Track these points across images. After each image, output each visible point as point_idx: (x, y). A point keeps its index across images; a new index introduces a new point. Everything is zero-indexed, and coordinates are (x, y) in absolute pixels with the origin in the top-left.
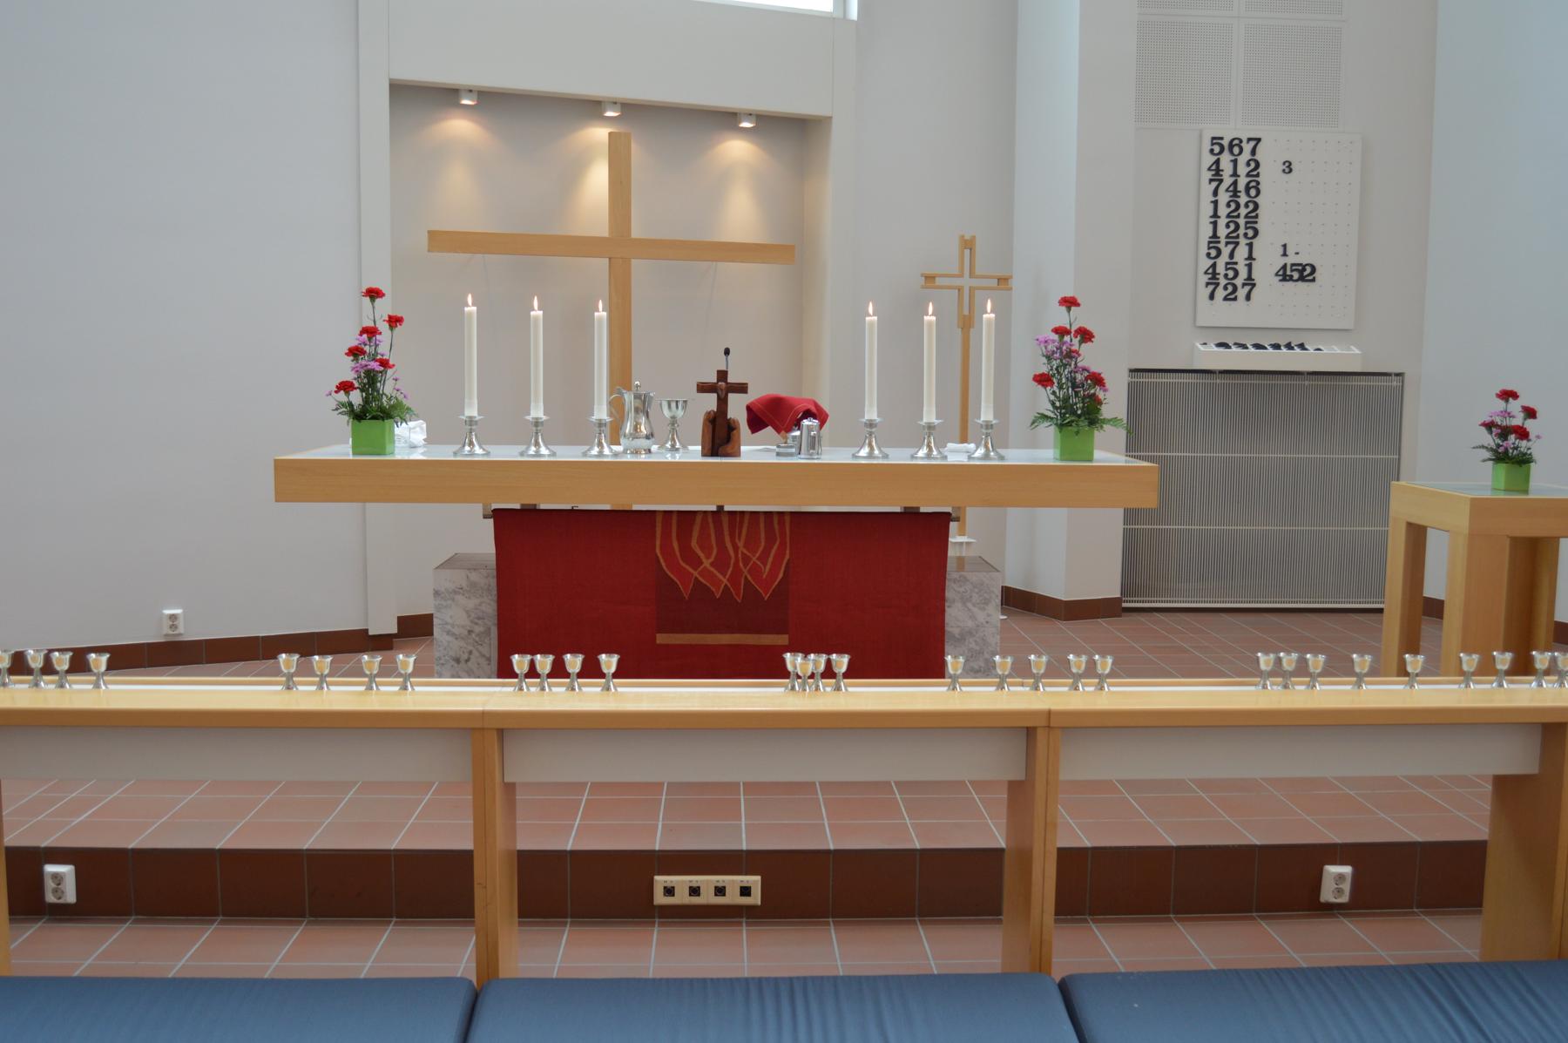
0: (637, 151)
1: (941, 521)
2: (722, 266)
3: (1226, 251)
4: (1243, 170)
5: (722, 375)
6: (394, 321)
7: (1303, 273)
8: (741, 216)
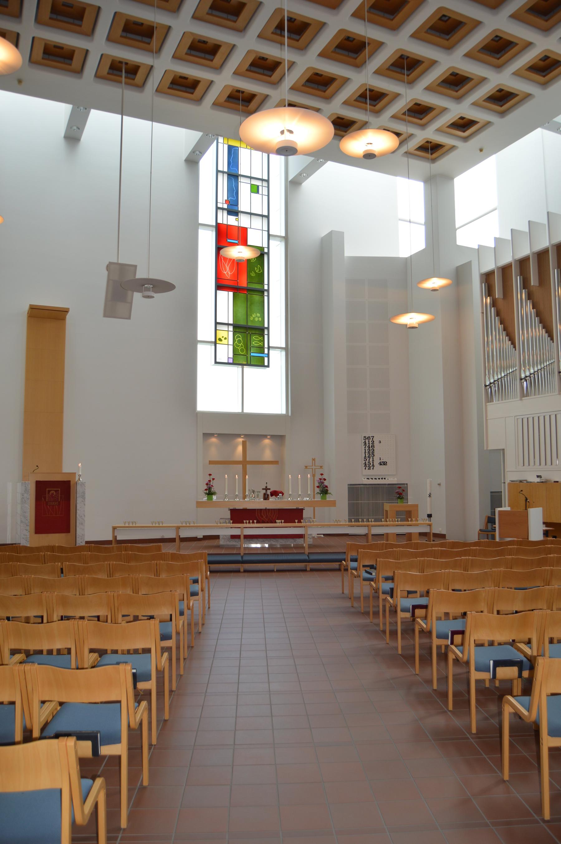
0: (248, 444)
1: (302, 510)
2: (264, 465)
3: (368, 459)
4: (371, 443)
5: (266, 487)
6: (213, 479)
7: (385, 463)
8: (268, 455)
